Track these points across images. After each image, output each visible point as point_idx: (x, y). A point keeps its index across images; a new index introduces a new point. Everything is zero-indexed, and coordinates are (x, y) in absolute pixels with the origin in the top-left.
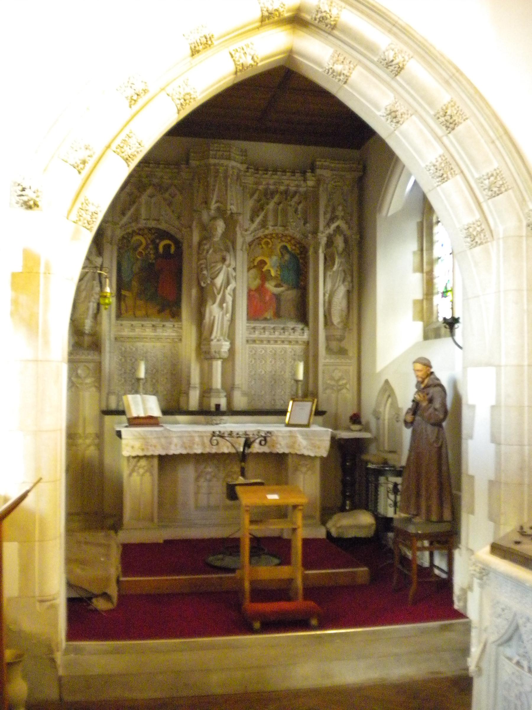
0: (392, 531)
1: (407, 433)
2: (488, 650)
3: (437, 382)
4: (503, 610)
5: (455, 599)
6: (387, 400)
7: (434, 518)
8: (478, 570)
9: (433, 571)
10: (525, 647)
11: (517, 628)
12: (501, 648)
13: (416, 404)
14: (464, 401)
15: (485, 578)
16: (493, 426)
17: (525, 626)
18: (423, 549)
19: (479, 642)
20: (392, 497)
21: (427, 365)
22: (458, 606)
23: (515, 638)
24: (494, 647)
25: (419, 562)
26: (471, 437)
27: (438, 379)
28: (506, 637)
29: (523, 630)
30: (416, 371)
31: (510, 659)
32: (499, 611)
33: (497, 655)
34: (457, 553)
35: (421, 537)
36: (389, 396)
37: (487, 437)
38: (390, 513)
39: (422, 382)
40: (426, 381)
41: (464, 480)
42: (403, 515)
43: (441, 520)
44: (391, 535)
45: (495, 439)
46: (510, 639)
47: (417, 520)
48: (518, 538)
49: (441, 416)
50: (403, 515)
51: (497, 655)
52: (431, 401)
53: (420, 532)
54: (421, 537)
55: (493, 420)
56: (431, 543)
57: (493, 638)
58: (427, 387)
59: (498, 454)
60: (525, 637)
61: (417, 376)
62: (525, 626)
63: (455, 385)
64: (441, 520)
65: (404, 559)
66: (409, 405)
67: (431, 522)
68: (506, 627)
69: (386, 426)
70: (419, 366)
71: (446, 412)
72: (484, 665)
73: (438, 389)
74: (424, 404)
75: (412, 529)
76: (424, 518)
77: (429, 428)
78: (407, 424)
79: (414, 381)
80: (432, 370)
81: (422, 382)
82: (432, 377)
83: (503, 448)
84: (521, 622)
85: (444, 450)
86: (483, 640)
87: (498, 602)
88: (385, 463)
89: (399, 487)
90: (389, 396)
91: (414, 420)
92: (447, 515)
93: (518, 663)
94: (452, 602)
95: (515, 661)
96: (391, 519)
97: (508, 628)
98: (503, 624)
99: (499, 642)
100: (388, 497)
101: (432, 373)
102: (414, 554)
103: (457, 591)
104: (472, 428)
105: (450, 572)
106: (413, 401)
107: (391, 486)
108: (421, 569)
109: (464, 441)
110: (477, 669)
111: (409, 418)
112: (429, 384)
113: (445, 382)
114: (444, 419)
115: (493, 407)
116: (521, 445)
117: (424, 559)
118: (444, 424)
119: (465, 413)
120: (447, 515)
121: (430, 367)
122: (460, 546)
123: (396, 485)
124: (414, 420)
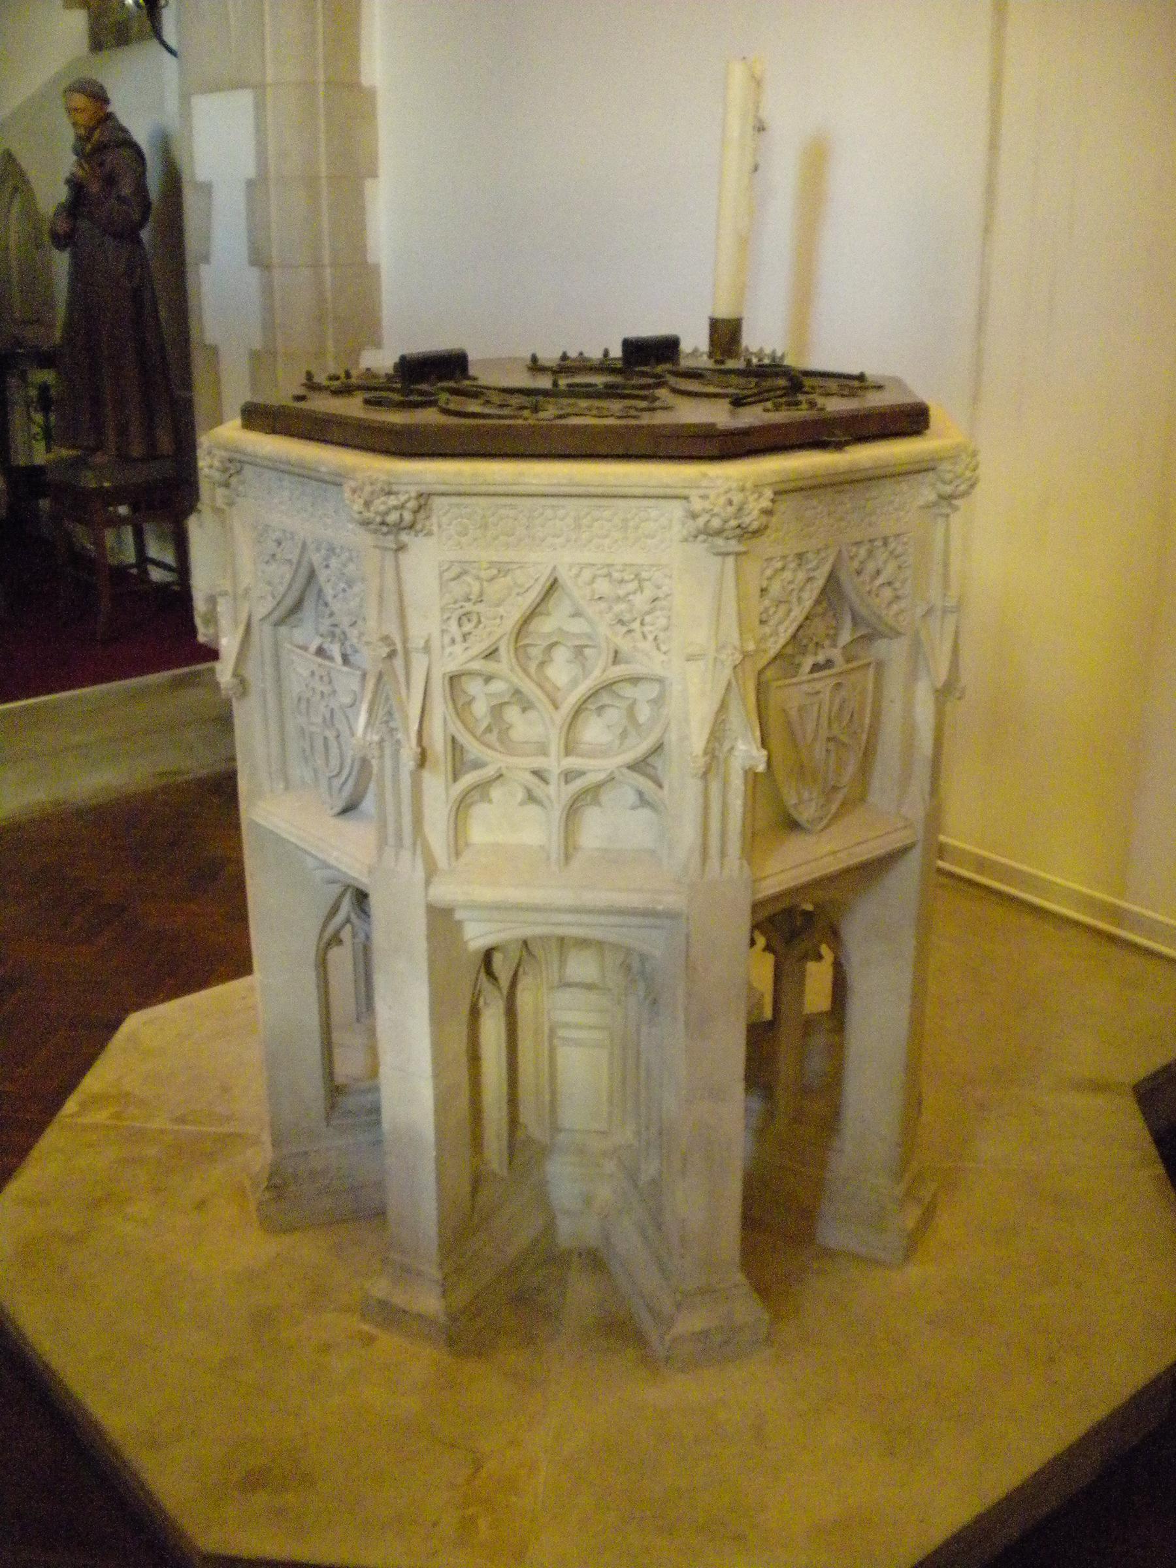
0: (45, 496)
1: (61, 262)
2: (255, 638)
3: (121, 135)
4: (279, 543)
5: (198, 621)
6: (10, 203)
7: (136, 451)
8: (217, 463)
9: (146, 572)
10: (332, 614)
11: (312, 575)
12: (283, 630)
13: (76, 186)
14: (186, 177)
15: (234, 480)
16: (251, 230)
17: (327, 566)
18: (116, 522)
19: (236, 622)
20: (39, 418)
21: (99, 97)
22: (205, 635)
23: (309, 604)
24: (267, 628)
25: (112, 561)
26: (206, 258)
27: (124, 130)
28: (289, 602)
29: (322, 575)
30: (71, 110)
31: (305, 648)
32: (271, 545)
33: (276, 647)
34: (194, 526)
35: (116, 496)
36: (16, 189)
37: (241, 249)
38: (40, 456)
39: (88, 138)
40: (96, 135)
41: (199, 362)
42: (65, 453)
43: (152, 455)
44: (44, 504)
45: (259, 259)
46: (297, 606)
47: (99, 459)
48: (302, 391)
49: (136, 217)
50: (65, 453)
51: (276, 647)
52: (110, 181)
53: (106, 484)
54: (116, 496)
55: (251, 212)
56: (135, 508)
57: (262, 610)
58: (101, 148)
59: (267, 290)
60: (329, 591)
61: (75, 124)
62: (327, 566)
63: (165, 145)
64: (152, 455)
65: (78, 558)
66: (62, 194)
67: (135, 460)
68: (288, 577)
69: (14, 263)
70: (80, 100)
71: (146, 206)
72: (251, 672)
73: (125, 152)
74: (94, 188)
75: (89, 480)
76: (114, 452)
77: (110, 243)
78: (61, 240)
79: (67, 136)
80: (110, 109)
81: (88, 138)
82: (110, 124)
83: (277, 273)
84: (316, 558)
85: (147, 295)
86: (243, 617)
87: (267, 527)
88: (18, 343)
89: (53, 392)
90: (16, 189)
91: (74, 230)
92: (165, 442)
93: (320, 652)
94: (193, 631)
95: (313, 647)
96: (40, 470)
97: (293, 579)
98: (282, 573)
99: (276, 615)
100: (30, 418)
101: (110, 117)
102: (99, 543)
103: (200, 605)
104: (207, 238)
105: (183, 569)
106: (68, 182)
107: (33, 393)
108: (120, 573)
109: (190, 269)
110: (236, 681)
111: (63, 227)
112: (105, 145)
113: (141, 135)
114: (141, 224)
115: (250, 184)
116: (316, 265)
117: (121, 547)
118: (145, 235)
119: (191, 200)
120: (165, 442)
121: (106, 101)
122: (199, 506)
123: (44, 389)
124: (74, 230)
